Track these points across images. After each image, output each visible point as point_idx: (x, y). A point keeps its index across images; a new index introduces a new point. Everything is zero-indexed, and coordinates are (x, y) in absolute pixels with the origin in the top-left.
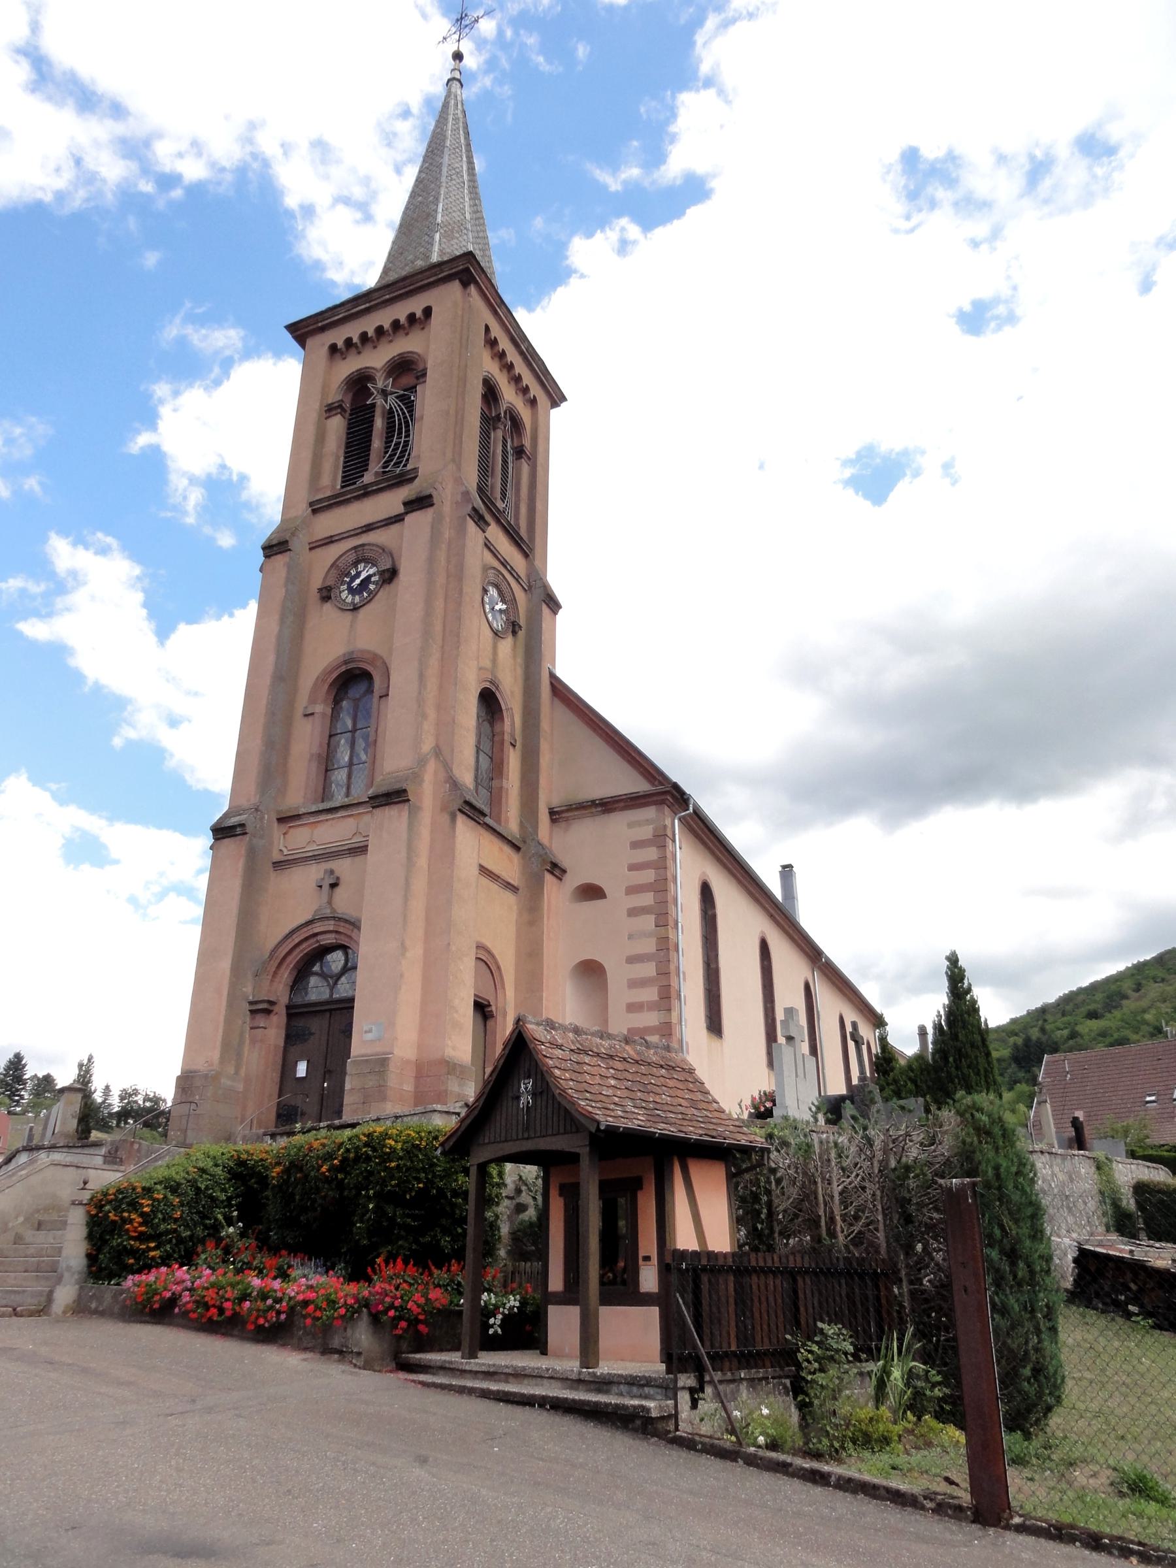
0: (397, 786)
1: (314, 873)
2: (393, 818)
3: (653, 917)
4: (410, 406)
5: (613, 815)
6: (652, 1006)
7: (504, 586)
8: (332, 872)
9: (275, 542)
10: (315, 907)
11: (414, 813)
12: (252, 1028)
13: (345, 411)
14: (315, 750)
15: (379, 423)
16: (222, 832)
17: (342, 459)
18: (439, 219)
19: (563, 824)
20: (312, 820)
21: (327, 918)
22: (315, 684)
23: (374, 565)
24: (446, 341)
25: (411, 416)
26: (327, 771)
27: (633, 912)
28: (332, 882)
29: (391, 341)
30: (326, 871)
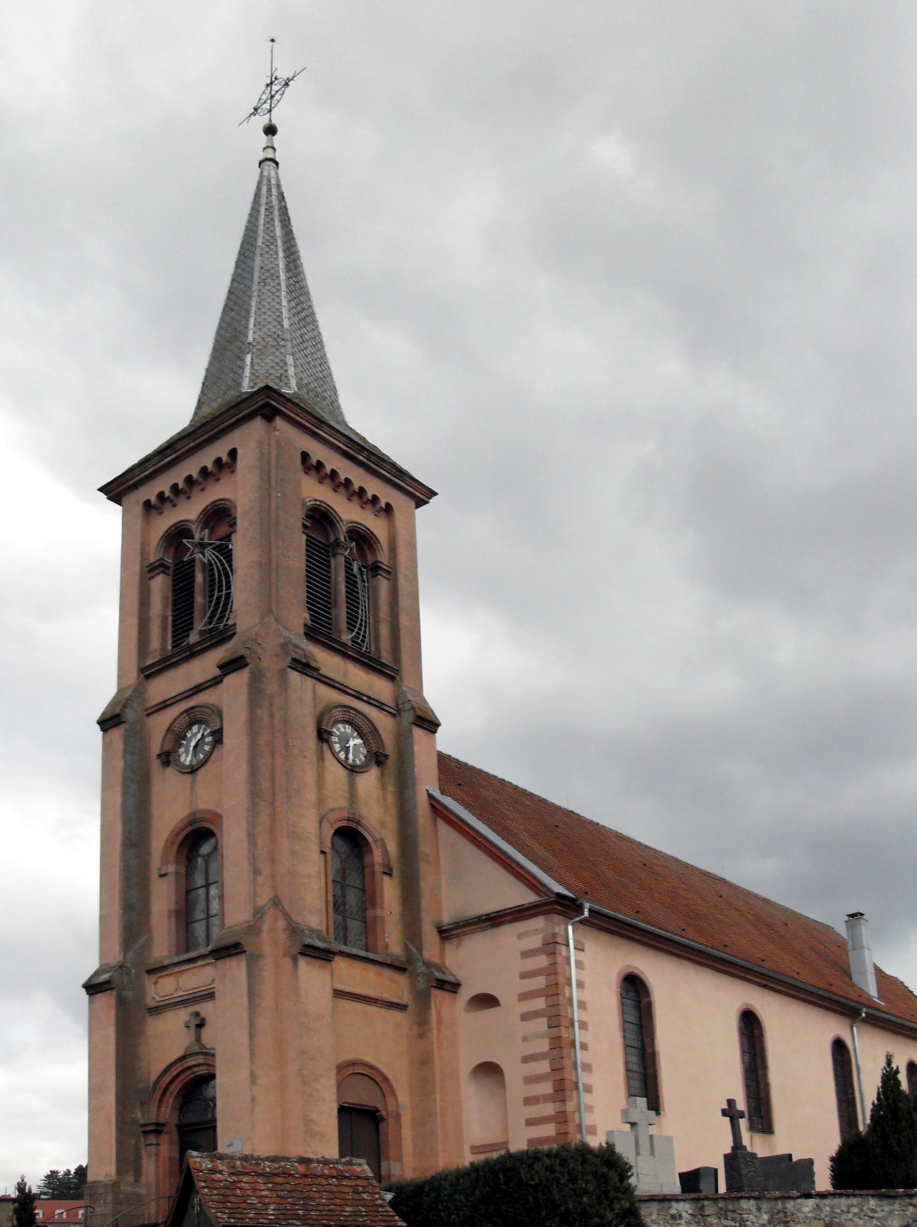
0: (231, 941)
1: (183, 1015)
2: (236, 968)
3: (545, 1020)
4: (228, 555)
5: (503, 928)
6: (547, 1099)
7: (358, 720)
8: (197, 1014)
9: (107, 717)
10: (186, 1044)
11: (253, 962)
12: (146, 1145)
13: (168, 568)
14: (173, 907)
15: (199, 578)
16: (92, 988)
17: (170, 619)
18: (250, 339)
19: (455, 941)
20: (177, 969)
21: (197, 1054)
22: (165, 846)
23: (208, 726)
24: (258, 481)
25: (231, 566)
26: (188, 924)
27: (526, 1017)
28: (198, 1022)
29: (203, 490)
30: (191, 1014)
